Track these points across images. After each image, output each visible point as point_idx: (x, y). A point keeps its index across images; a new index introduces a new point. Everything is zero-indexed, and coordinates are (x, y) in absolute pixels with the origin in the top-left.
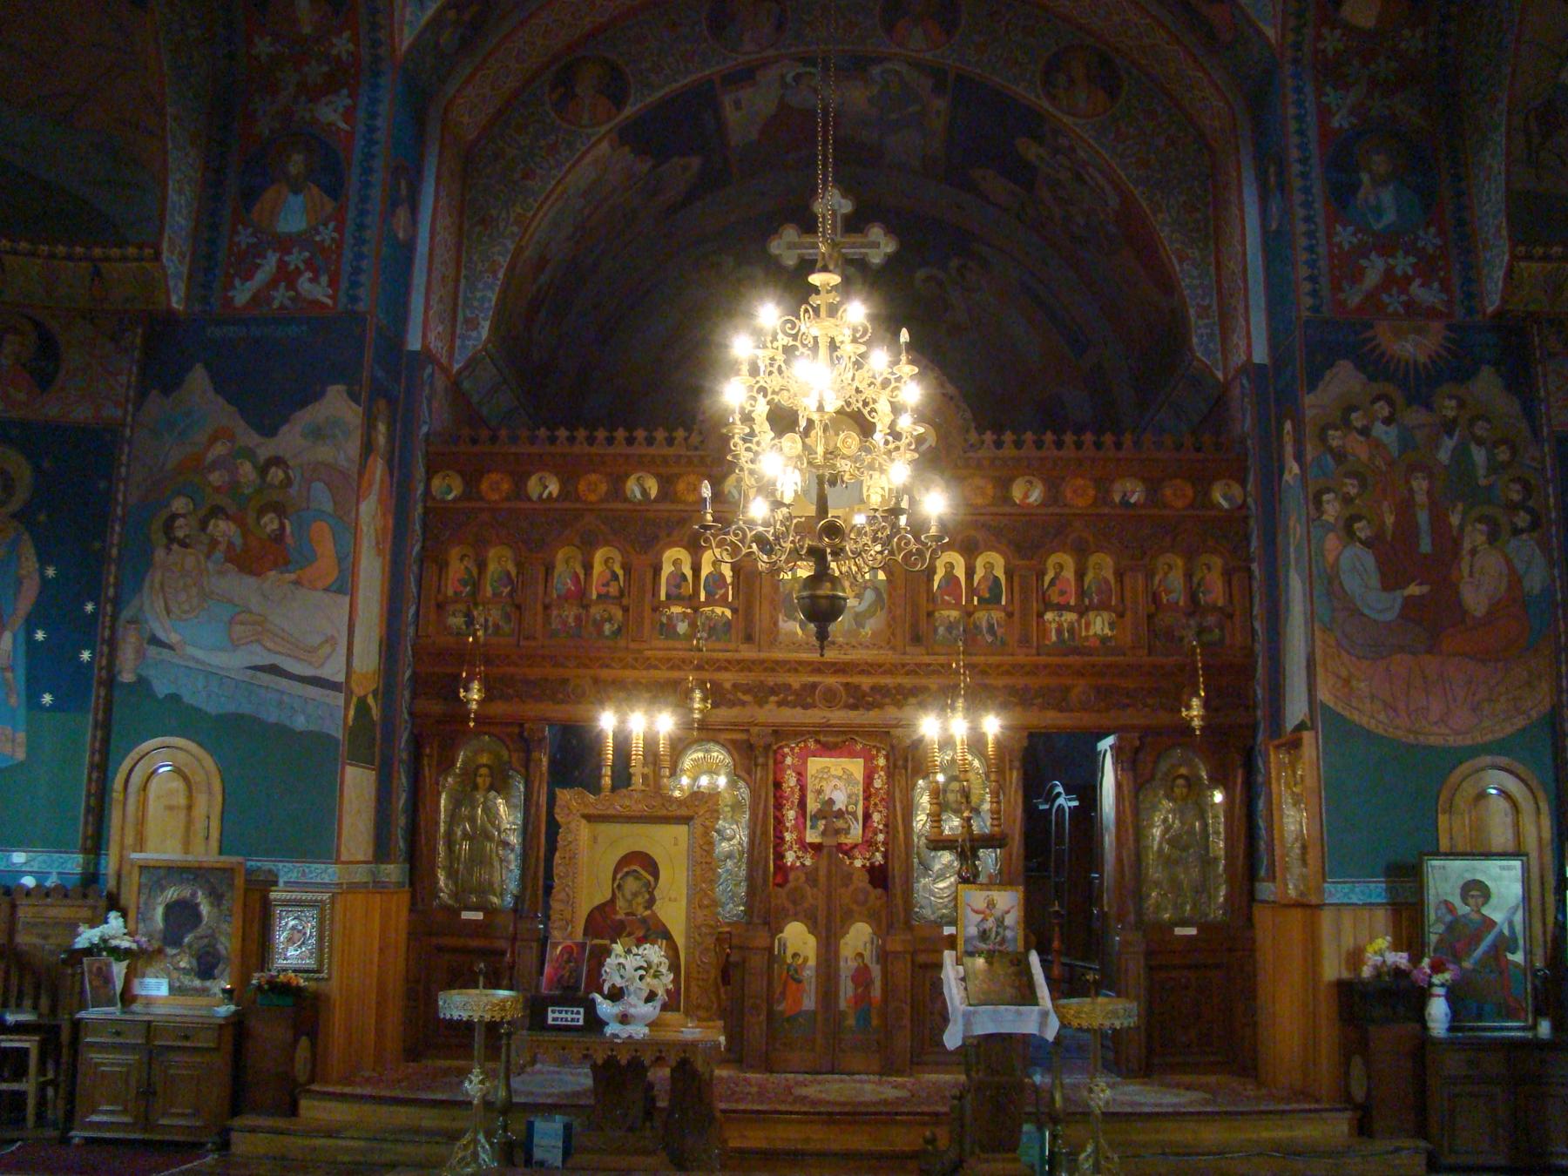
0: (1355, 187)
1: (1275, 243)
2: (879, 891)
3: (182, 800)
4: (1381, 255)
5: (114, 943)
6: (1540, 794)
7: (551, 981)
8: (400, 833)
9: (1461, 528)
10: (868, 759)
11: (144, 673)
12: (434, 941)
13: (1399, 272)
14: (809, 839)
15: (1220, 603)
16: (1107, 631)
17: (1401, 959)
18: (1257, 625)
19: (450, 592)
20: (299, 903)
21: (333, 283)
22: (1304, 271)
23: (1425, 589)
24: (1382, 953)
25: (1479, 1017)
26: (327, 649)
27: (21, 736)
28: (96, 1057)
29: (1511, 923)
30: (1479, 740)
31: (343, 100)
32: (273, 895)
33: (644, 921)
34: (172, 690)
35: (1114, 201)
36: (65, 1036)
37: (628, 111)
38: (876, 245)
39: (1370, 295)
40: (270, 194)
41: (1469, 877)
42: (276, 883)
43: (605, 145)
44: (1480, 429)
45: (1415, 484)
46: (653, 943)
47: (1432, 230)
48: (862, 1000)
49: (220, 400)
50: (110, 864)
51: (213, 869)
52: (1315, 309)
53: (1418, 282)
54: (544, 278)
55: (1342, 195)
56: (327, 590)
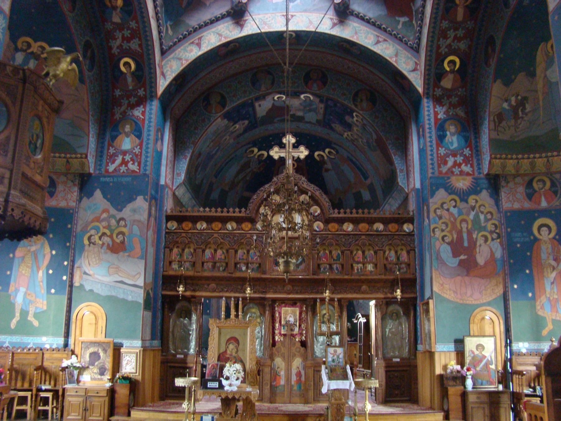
0: (444, 136)
1: (422, 151)
2: (303, 348)
3: (94, 322)
4: (452, 157)
5: (75, 365)
6: (500, 318)
7: (208, 374)
8: (159, 332)
9: (476, 239)
10: (301, 308)
11: (81, 283)
12: (169, 364)
13: (458, 162)
14: (282, 333)
15: (406, 260)
16: (372, 269)
17: (458, 367)
18: (417, 267)
19: (173, 258)
20: (130, 353)
21: (139, 165)
22: (430, 162)
23: (466, 257)
24: (454, 366)
25: (482, 384)
26: (138, 276)
27: (45, 302)
28: (70, 399)
29: (491, 357)
30: (482, 302)
31: (141, 109)
32: (122, 350)
33: (235, 357)
34: (91, 288)
35: (375, 136)
36: (60, 393)
37: (227, 109)
38: (302, 152)
39: (449, 169)
40: (119, 138)
41: (478, 343)
42: (123, 347)
43: (219, 119)
44: (482, 209)
45: (462, 226)
46: (238, 363)
47: (468, 149)
48: (299, 381)
49: (105, 201)
50: (71, 341)
51: (104, 343)
52: (433, 173)
53: (464, 165)
54: (200, 160)
55: (441, 138)
56: (138, 258)
